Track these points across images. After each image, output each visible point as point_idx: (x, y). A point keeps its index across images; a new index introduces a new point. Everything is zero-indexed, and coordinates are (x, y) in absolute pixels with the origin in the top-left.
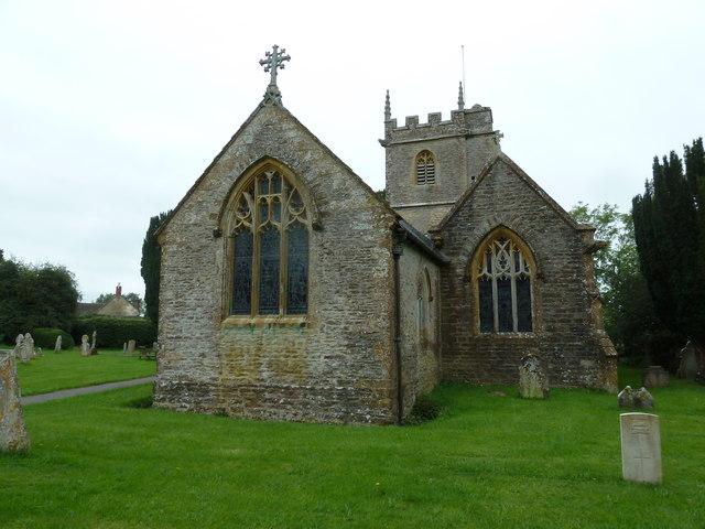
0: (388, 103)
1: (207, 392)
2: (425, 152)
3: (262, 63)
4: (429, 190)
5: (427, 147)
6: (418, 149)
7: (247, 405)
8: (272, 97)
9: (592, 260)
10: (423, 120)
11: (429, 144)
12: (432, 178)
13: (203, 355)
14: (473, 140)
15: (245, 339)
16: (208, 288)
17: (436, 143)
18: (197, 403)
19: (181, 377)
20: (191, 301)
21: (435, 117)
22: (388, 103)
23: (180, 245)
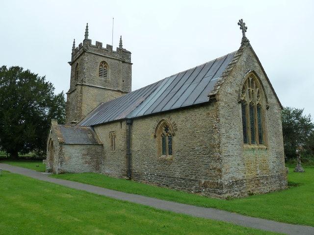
0: (87, 29)
1: (243, 184)
2: (104, 62)
3: (242, 20)
4: (105, 81)
5: (106, 60)
6: (102, 59)
7: (256, 187)
8: (245, 42)
9: (294, 133)
10: (104, 46)
11: (106, 59)
12: (105, 76)
13: (238, 164)
14: (124, 64)
15: (250, 154)
16: (237, 129)
17: (110, 60)
18: (240, 191)
19: (232, 178)
20: (232, 136)
21: (109, 47)
22: (87, 29)
23: (226, 103)
